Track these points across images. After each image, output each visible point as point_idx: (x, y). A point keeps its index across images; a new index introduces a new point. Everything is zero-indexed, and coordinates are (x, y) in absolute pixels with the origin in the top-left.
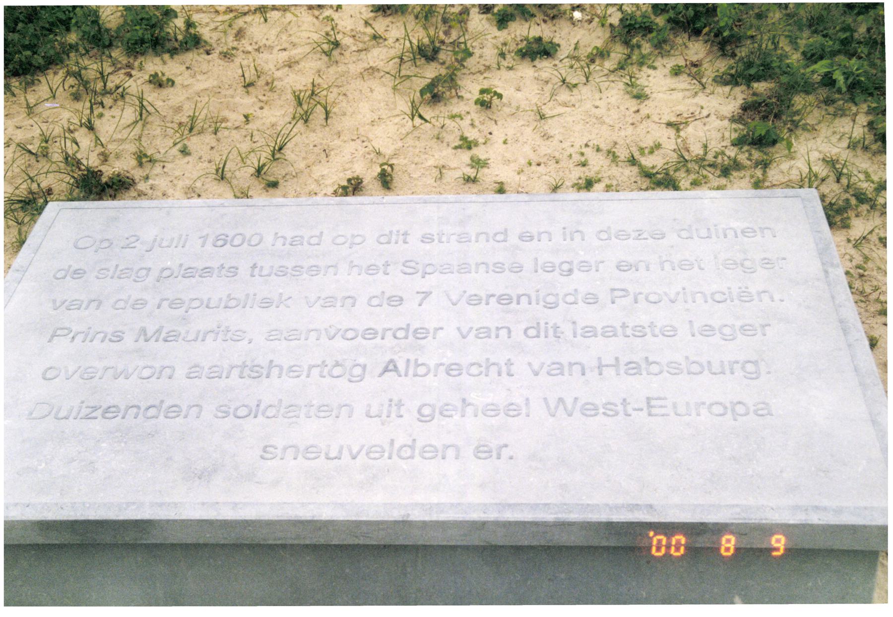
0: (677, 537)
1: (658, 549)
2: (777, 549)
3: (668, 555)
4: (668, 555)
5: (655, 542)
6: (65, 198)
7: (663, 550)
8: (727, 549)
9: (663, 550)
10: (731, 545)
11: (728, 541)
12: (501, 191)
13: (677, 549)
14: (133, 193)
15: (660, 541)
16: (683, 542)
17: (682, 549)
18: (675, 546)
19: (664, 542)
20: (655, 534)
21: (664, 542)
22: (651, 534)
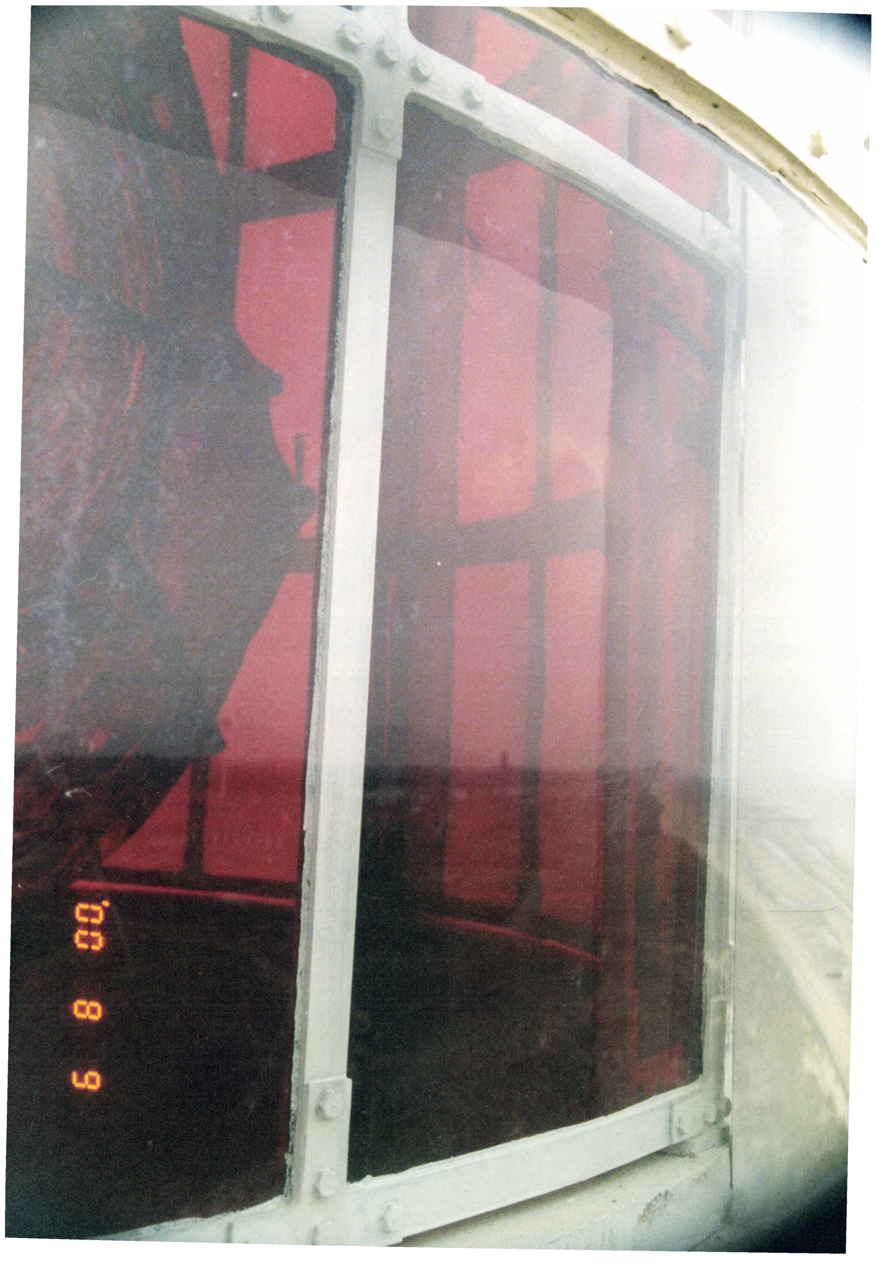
0: (101, 940)
1: (84, 913)
2: (81, 1079)
3: (101, 928)
4: (101, 928)
5: (95, 908)
6: (309, 577)
7: (85, 919)
8: (82, 1009)
9: (85, 919)
10: (87, 1015)
11: (94, 1011)
12: (716, 106)
13: (83, 939)
14: (422, 90)
15: (95, 914)
16: (95, 948)
17: (85, 946)
18: (89, 936)
19: (94, 921)
20: (104, 908)
21: (94, 921)
22: (106, 904)
